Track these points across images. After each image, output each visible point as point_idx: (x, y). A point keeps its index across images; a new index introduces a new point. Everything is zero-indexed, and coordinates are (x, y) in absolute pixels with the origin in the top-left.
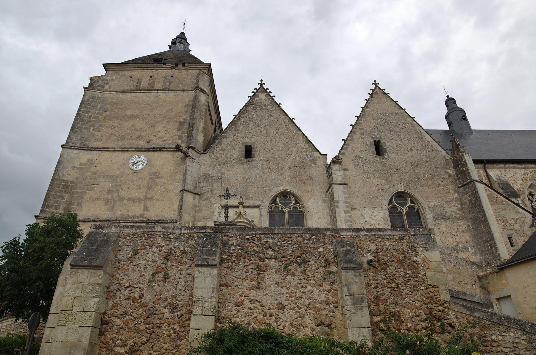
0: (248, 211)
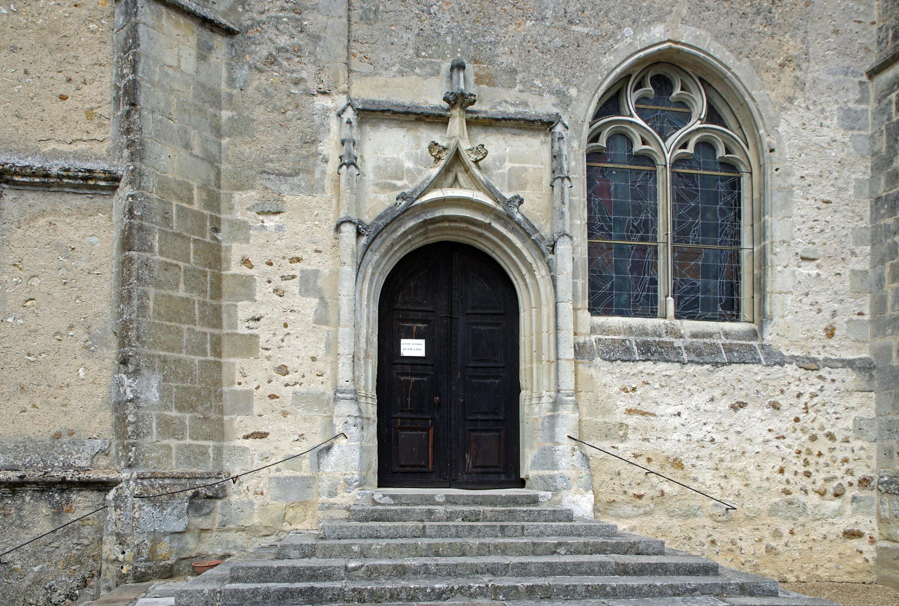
0: (497, 145)
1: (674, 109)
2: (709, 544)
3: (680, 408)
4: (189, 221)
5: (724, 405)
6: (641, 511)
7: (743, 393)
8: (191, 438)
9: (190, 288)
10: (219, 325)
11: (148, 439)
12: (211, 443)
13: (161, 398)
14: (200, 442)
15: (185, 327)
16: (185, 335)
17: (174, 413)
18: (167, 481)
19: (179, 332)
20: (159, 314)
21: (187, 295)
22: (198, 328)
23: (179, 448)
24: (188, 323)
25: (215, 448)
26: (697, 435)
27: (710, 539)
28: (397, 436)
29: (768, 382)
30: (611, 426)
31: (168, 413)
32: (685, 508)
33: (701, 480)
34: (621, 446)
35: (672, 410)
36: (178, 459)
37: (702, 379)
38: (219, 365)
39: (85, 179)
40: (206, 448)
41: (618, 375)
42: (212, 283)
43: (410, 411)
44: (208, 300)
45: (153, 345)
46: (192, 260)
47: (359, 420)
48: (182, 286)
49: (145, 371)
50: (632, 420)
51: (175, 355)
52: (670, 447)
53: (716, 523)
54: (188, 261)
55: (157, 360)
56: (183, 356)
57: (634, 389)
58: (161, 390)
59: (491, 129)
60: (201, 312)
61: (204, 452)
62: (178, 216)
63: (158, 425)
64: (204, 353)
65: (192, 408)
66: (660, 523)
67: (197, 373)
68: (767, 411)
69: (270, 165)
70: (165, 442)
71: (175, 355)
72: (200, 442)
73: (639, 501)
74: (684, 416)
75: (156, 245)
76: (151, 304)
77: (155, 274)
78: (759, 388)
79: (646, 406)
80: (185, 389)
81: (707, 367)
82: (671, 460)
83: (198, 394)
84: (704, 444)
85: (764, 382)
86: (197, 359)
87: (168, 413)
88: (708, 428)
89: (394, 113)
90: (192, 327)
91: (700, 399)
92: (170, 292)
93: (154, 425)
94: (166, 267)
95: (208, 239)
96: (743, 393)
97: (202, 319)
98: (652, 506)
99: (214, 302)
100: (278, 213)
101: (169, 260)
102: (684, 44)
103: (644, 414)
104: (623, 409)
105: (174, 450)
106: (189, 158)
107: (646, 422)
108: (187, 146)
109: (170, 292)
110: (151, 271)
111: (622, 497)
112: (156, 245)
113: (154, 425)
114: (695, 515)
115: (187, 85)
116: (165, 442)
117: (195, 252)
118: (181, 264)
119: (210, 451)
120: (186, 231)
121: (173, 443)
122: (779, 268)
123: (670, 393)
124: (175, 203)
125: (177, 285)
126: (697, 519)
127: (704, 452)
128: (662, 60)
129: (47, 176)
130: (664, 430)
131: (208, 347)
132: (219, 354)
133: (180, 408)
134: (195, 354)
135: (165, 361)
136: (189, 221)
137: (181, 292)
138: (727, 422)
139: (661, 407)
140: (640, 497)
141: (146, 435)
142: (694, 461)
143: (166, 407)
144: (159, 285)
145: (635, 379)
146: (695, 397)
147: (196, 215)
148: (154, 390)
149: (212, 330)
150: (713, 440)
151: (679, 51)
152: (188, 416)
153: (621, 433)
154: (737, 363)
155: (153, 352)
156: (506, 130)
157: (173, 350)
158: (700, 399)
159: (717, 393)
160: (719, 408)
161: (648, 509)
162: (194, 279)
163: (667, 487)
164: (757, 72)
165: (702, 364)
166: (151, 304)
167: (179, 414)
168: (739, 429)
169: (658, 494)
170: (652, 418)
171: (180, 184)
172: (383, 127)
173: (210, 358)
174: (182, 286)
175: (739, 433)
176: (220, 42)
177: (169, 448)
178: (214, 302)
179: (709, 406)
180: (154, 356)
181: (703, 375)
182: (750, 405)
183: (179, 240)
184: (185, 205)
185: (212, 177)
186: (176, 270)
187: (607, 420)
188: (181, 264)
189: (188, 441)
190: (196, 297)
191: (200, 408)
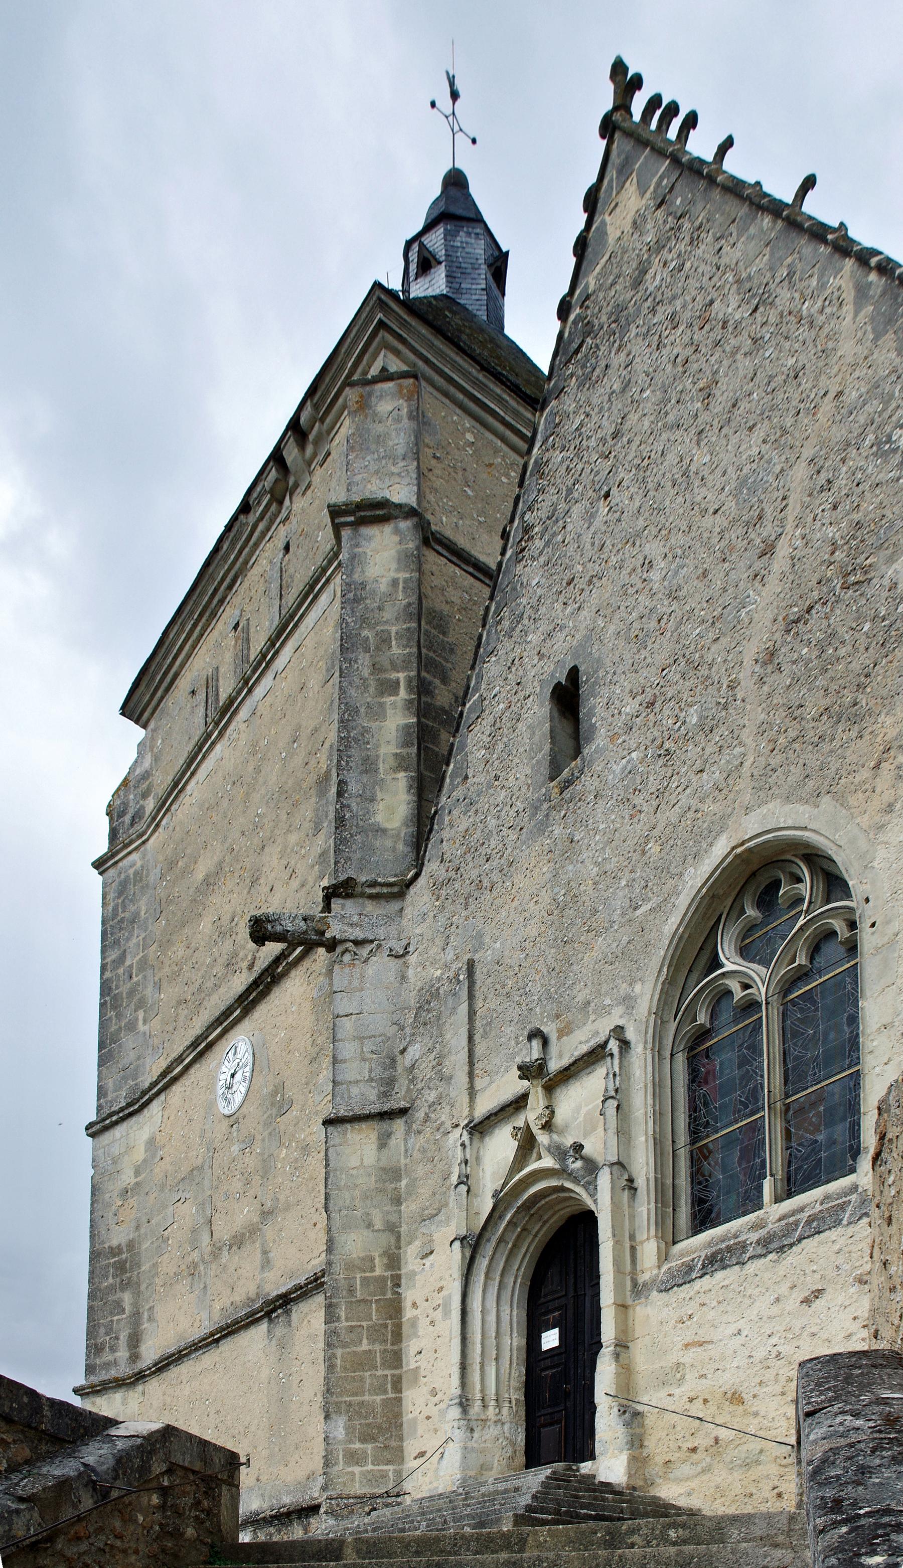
1: (787, 917)
2: (775, 1499)
3: (739, 1325)
4: (372, 1287)
5: (793, 1302)
6: (699, 1469)
7: (817, 1276)
8: (373, 1464)
9: (372, 1341)
10: (400, 1366)
11: (336, 1468)
12: (390, 1467)
13: (347, 1434)
14: (381, 1468)
15: (367, 1374)
16: (368, 1381)
17: (358, 1445)
18: (351, 1501)
19: (362, 1380)
20: (346, 1369)
21: (370, 1347)
22: (380, 1373)
23: (362, 1473)
24: (370, 1370)
25: (395, 1471)
26: (760, 1354)
27: (776, 1491)
28: (540, 1433)
29: (851, 1248)
30: (668, 1370)
31: (352, 1446)
32: (743, 1456)
33: (762, 1413)
34: (677, 1392)
35: (732, 1329)
36: (361, 1482)
37: (767, 1275)
38: (399, 1400)
39: (316, 1280)
40: (387, 1471)
41: (674, 1305)
42: (392, 1332)
43: (549, 1406)
44: (389, 1347)
45: (341, 1394)
46: (374, 1317)
47: (462, 1422)
48: (365, 1341)
49: (333, 1416)
50: (688, 1357)
51: (359, 1398)
52: (727, 1380)
53: (782, 1469)
54: (371, 1319)
55: (343, 1405)
56: (366, 1398)
57: (690, 1317)
58: (346, 1428)
59: (571, 1081)
60: (382, 1359)
61: (384, 1475)
62: (362, 1285)
63: (344, 1456)
64: (385, 1392)
65: (374, 1439)
66: (719, 1480)
67: (379, 1410)
68: (852, 1290)
69: (426, 1212)
70: (350, 1469)
71: (359, 1398)
72: (381, 1468)
73: (695, 1457)
74: (744, 1333)
75: (343, 1314)
76: (339, 1362)
77: (342, 1337)
78: (840, 1260)
79: (703, 1335)
80: (367, 1425)
81: (771, 1256)
82: (729, 1395)
83: (379, 1427)
84: (770, 1363)
85: (846, 1249)
86: (378, 1399)
87: (352, 1446)
88: (774, 1340)
89: (496, 1114)
90: (374, 1372)
91: (763, 1305)
92: (355, 1349)
93: (341, 1457)
94: (351, 1329)
95: (389, 1295)
96: (817, 1276)
97: (383, 1364)
98: (708, 1459)
99: (395, 1347)
100: (432, 1252)
101: (353, 1324)
102: (750, 839)
103: (701, 1344)
104: (680, 1345)
105: (357, 1476)
106: (371, 1234)
107: (704, 1354)
108: (369, 1225)
109: (355, 1349)
110: (338, 1336)
111: (677, 1455)
112: (343, 1314)
113: (341, 1457)
114: (758, 1462)
115: (369, 1175)
116: (350, 1469)
117: (377, 1310)
118: (364, 1324)
119: (390, 1474)
120: (370, 1295)
121: (357, 1469)
122: (877, 1070)
123: (729, 1308)
124: (358, 1276)
125: (360, 1342)
126: (760, 1468)
127: (769, 1375)
128: (755, 867)
129: (301, 1288)
130: (723, 1358)
131: (389, 1386)
132: (400, 1391)
133: (363, 1440)
134: (377, 1394)
135: (350, 1405)
136: (372, 1287)
137: (365, 1346)
138: (797, 1324)
139: (720, 1329)
140: (694, 1450)
141: (334, 1465)
142: (756, 1390)
143: (351, 1442)
144: (345, 1345)
145: (692, 1303)
146: (757, 1304)
147: (383, 1279)
148: (341, 1429)
149: (393, 1372)
150: (778, 1355)
151: (750, 850)
152: (370, 1446)
153: (678, 1376)
154: (809, 1237)
155: (340, 1399)
156: (583, 1073)
157: (357, 1394)
158: (763, 1305)
159: (784, 1289)
160: (788, 1308)
161: (704, 1464)
162: (376, 1334)
163: (723, 1433)
164: (842, 805)
165: (765, 1255)
166: (339, 1362)
167: (362, 1446)
168: (813, 1330)
169: (712, 1442)
170: (710, 1347)
171: (363, 1259)
172: (497, 1131)
173: (391, 1395)
174: (365, 1341)
175: (814, 1335)
176: (399, 1125)
177: (353, 1474)
178: (395, 1347)
179: (775, 1310)
180: (341, 1402)
181: (767, 1269)
182: (828, 1290)
183: (362, 1304)
184: (368, 1274)
185: (393, 1241)
186: (360, 1330)
187: (663, 1364)
188: (364, 1324)
189: (370, 1467)
190: (378, 1347)
191: (381, 1439)
